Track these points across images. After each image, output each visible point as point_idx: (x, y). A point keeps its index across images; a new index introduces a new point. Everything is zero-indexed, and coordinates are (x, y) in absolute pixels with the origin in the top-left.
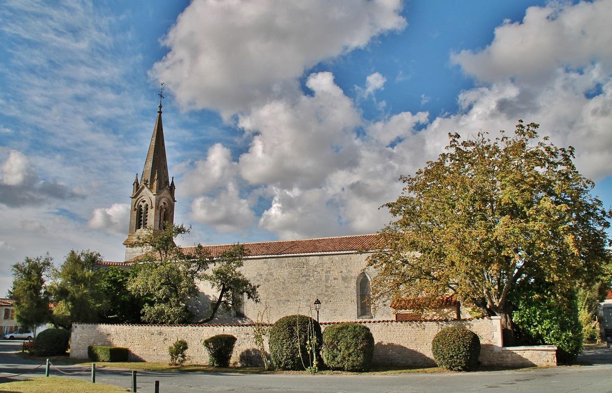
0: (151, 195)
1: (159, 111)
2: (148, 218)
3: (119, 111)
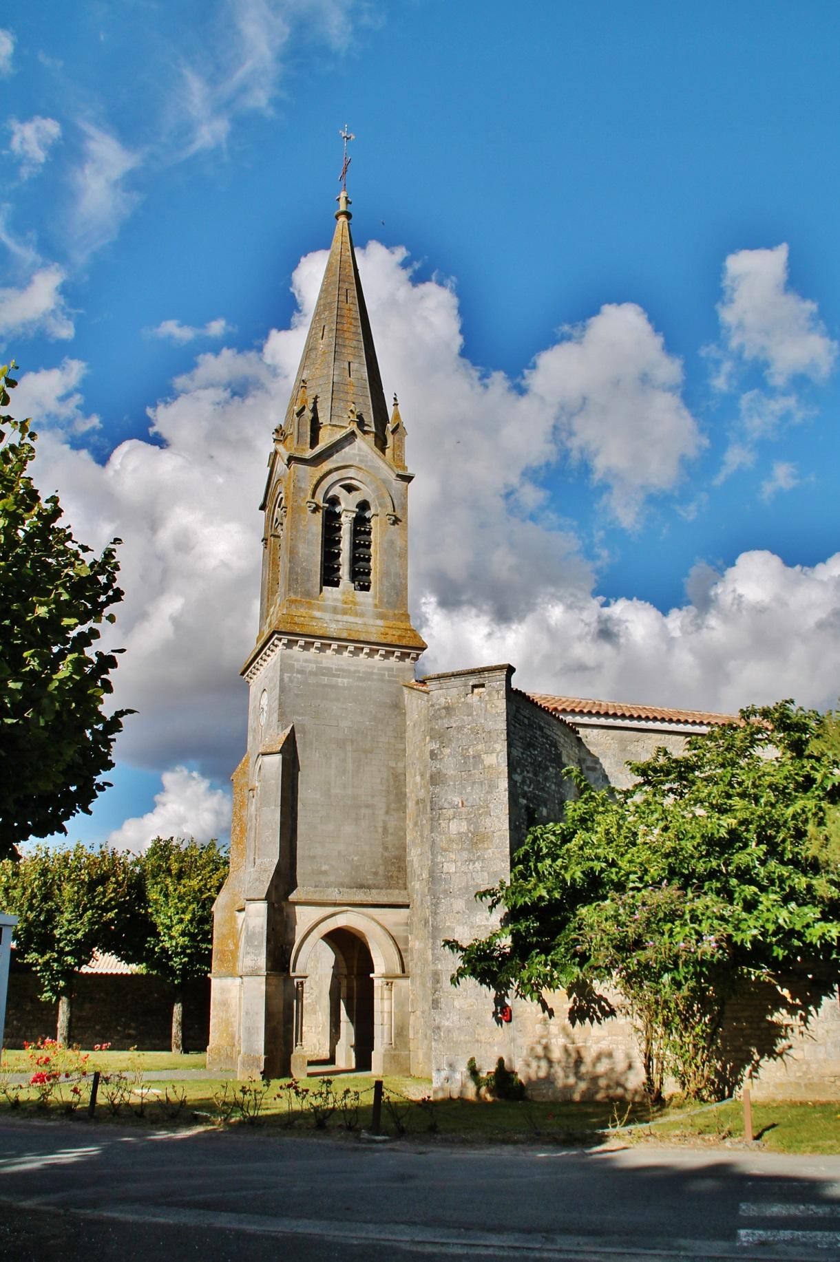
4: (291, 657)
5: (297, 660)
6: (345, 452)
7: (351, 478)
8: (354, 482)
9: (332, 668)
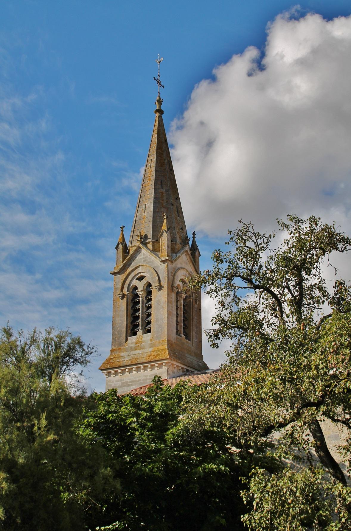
0: (156, 261)
1: (157, 108)
2: (153, 310)
3: (33, 239)
4: (110, 381)
5: (113, 382)
6: (137, 259)
7: (141, 272)
8: (142, 274)
9: (128, 382)
